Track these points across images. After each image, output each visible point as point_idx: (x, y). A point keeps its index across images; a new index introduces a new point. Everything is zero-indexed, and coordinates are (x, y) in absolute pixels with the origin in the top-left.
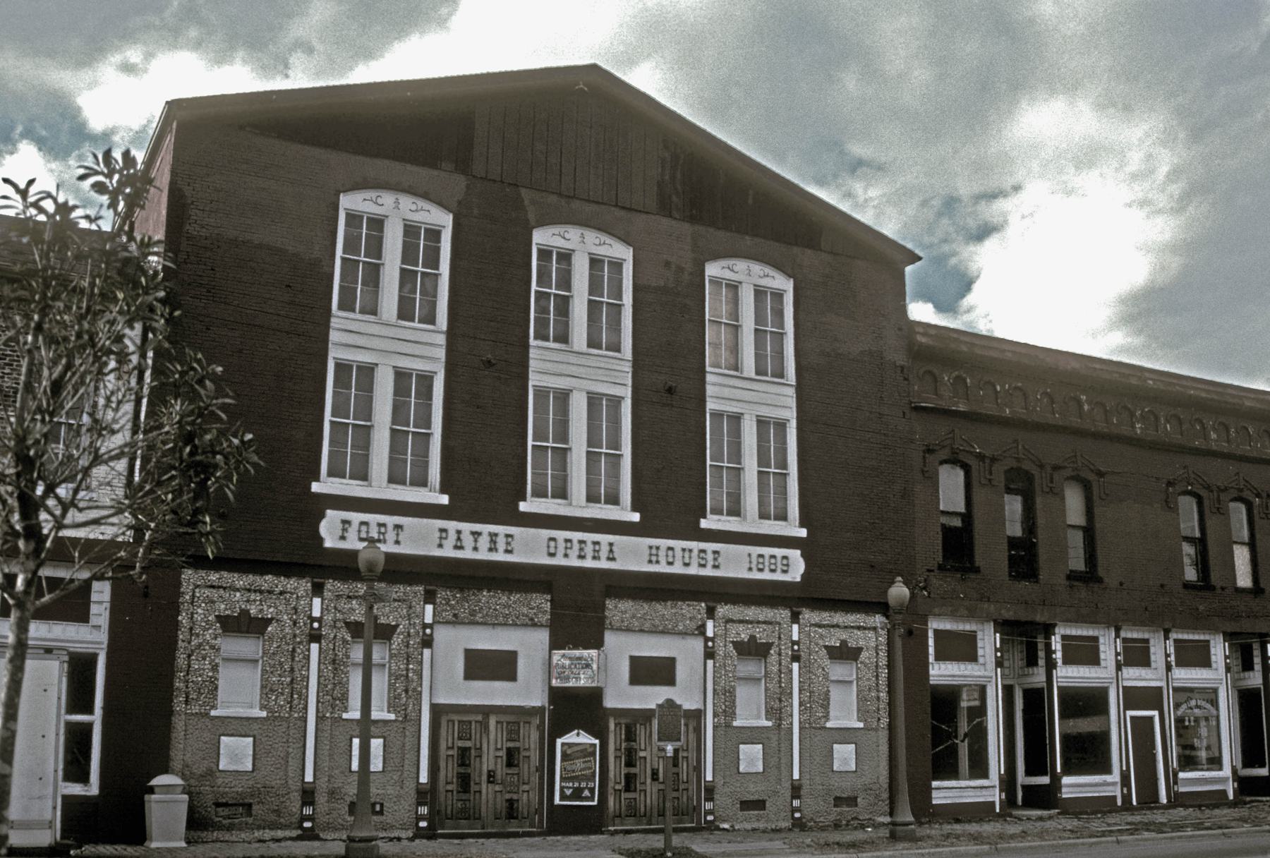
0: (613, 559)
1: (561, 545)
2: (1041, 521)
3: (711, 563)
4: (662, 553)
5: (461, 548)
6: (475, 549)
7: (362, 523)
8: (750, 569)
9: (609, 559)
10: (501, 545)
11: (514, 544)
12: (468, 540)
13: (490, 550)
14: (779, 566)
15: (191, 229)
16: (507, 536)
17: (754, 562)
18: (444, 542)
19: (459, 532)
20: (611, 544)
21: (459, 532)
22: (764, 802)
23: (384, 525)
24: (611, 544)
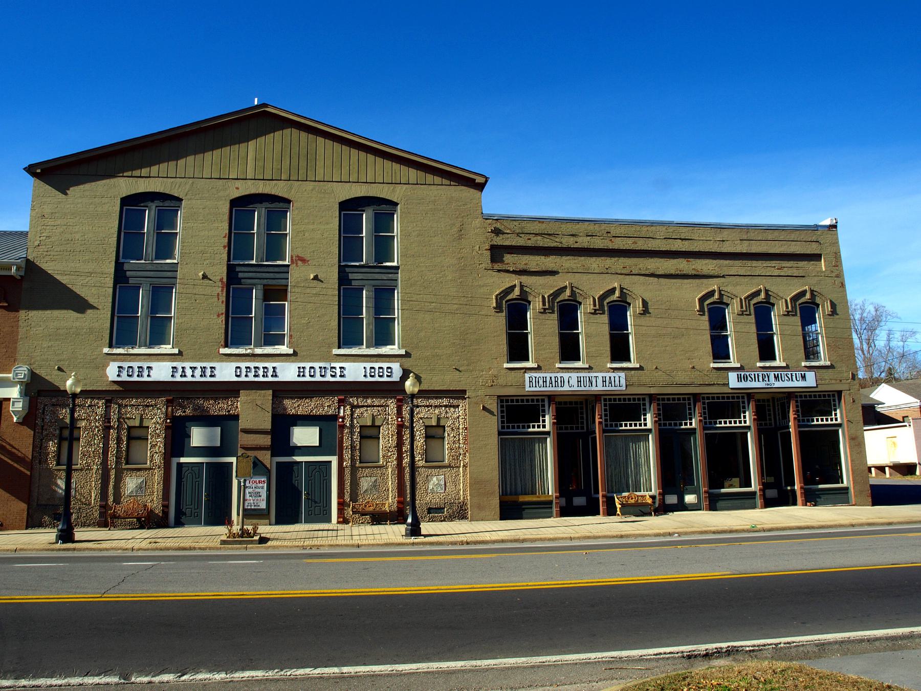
0: (276, 376)
1: (244, 370)
2: (283, 561)
3: (338, 374)
4: (307, 371)
5: (185, 376)
6: (149, 376)
7: (311, 368)
8: (365, 376)
9: (341, 376)
10: (208, 372)
11: (216, 372)
12: (189, 372)
13: (201, 376)
14: (386, 373)
15: (154, 502)
16: (211, 368)
17: (368, 371)
18: (175, 374)
19: (183, 368)
20: (274, 368)
21: (183, 368)
22: (464, 392)
23: (249, 367)
24: (274, 368)
